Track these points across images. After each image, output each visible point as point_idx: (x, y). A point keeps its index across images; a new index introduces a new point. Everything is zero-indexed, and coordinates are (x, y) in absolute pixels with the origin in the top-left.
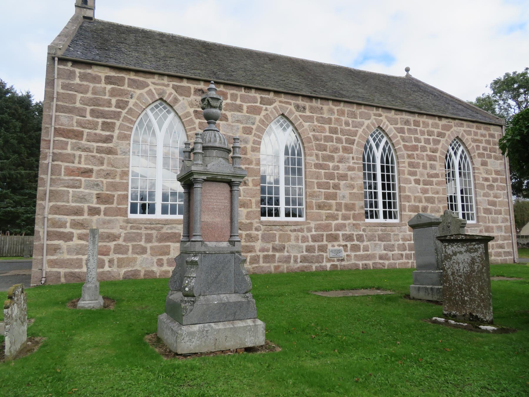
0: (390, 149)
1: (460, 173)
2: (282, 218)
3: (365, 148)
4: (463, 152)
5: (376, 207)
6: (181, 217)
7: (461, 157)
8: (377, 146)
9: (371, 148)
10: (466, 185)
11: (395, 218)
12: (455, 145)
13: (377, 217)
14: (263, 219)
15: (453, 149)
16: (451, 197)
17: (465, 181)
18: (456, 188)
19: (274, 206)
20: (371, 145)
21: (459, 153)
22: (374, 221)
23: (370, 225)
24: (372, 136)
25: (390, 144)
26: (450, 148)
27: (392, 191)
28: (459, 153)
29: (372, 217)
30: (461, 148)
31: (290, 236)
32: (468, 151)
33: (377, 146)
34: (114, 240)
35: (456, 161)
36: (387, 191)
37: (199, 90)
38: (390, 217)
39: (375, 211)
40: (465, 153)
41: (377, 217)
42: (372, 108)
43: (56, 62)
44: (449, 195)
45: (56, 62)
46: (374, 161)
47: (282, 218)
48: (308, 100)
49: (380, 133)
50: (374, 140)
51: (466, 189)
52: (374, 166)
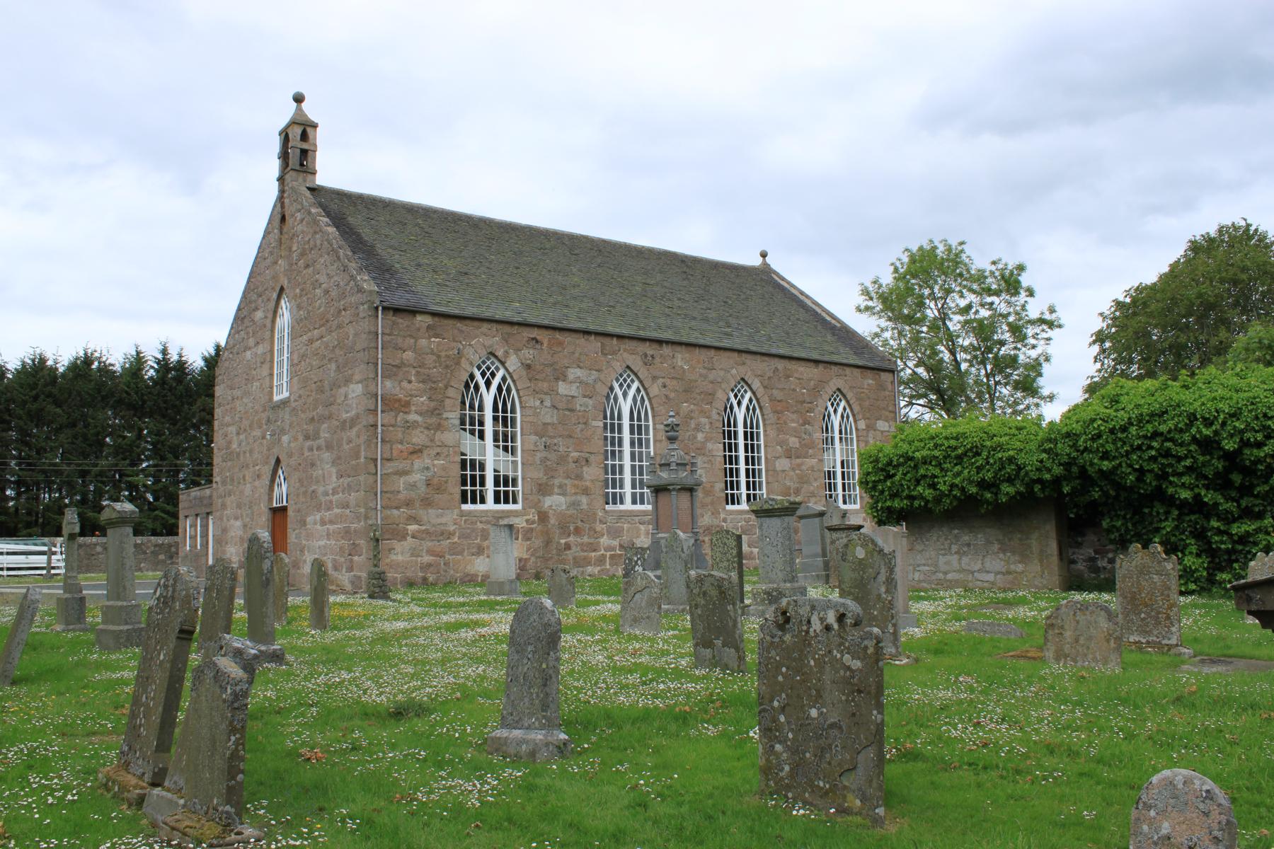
0: (509, 390)
1: (841, 439)
2: (490, 505)
3: (467, 386)
4: (751, 400)
5: (621, 487)
6: (649, 507)
7: (748, 409)
8: (488, 384)
9: (477, 387)
10: (848, 456)
11: (515, 502)
12: (625, 380)
13: (483, 501)
14: (465, 507)
15: (736, 396)
16: (829, 472)
17: (847, 450)
18: (835, 460)
19: (618, 490)
20: (616, 395)
21: (745, 402)
22: (736, 507)
23: (732, 512)
24: (479, 368)
25: (509, 380)
26: (732, 395)
27: (757, 467)
28: (745, 402)
29: (474, 501)
30: (843, 403)
31: (639, 529)
32: (509, 373)
33: (488, 384)
34: (449, 538)
35: (740, 414)
36: (750, 467)
37: (533, 339)
38: (506, 502)
39: (513, 491)
40: (848, 410)
41: (483, 501)
42: (693, 349)
43: (380, 312)
44: (826, 469)
45: (380, 312)
46: (620, 418)
47: (490, 505)
48: (655, 346)
49: (493, 363)
50: (483, 374)
51: (848, 461)
52: (620, 426)
